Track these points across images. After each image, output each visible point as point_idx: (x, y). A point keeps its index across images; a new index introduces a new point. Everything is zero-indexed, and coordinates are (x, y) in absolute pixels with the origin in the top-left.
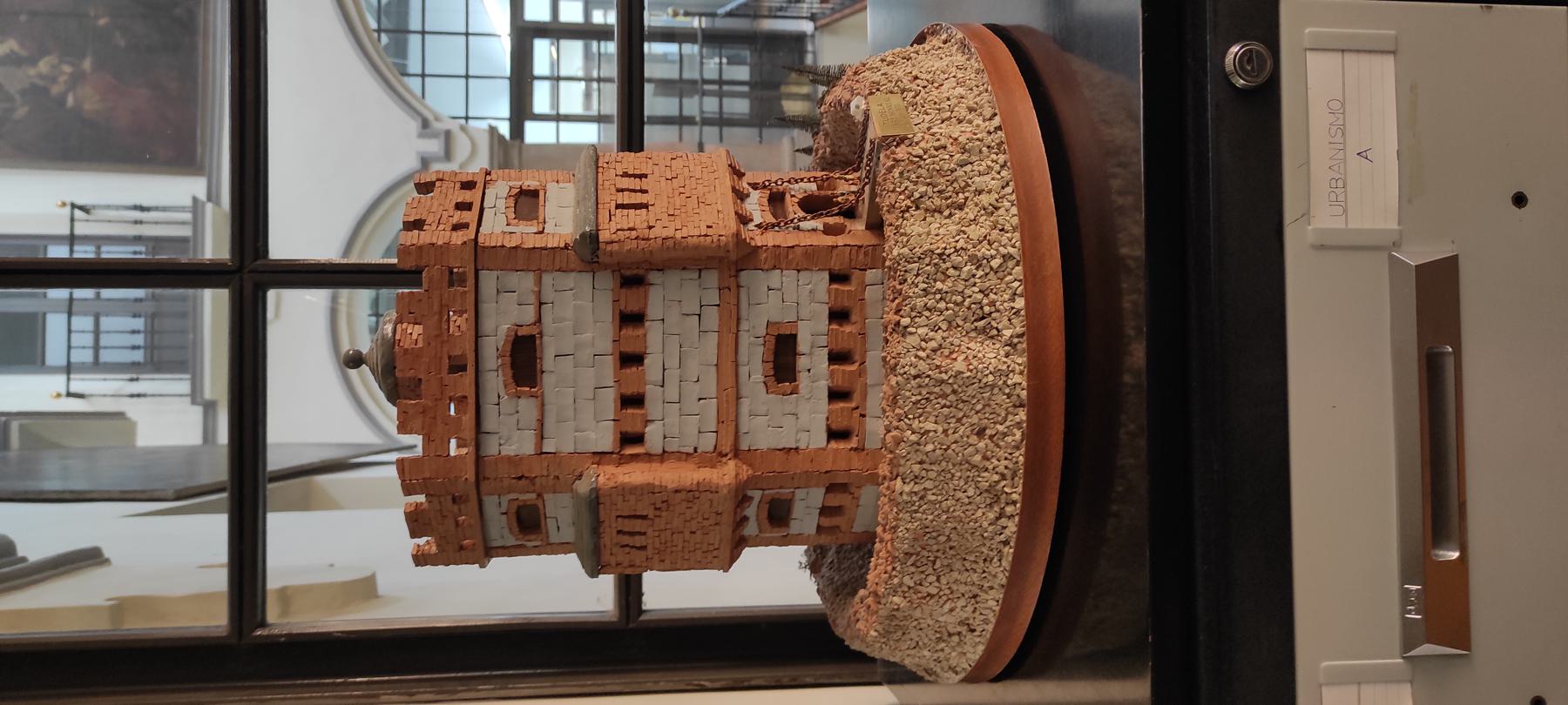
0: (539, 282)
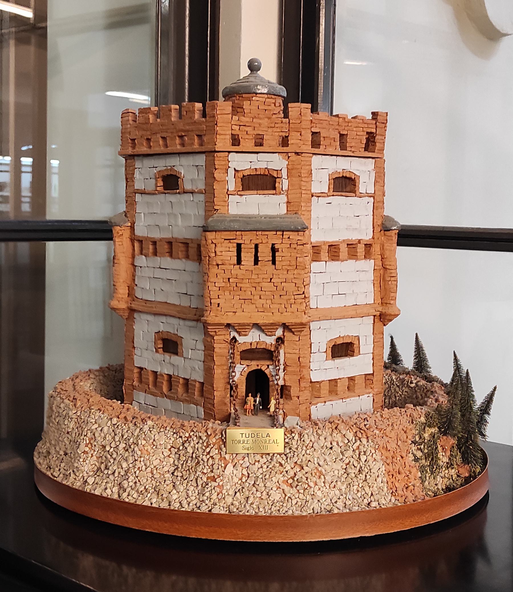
0: (200, 192)
